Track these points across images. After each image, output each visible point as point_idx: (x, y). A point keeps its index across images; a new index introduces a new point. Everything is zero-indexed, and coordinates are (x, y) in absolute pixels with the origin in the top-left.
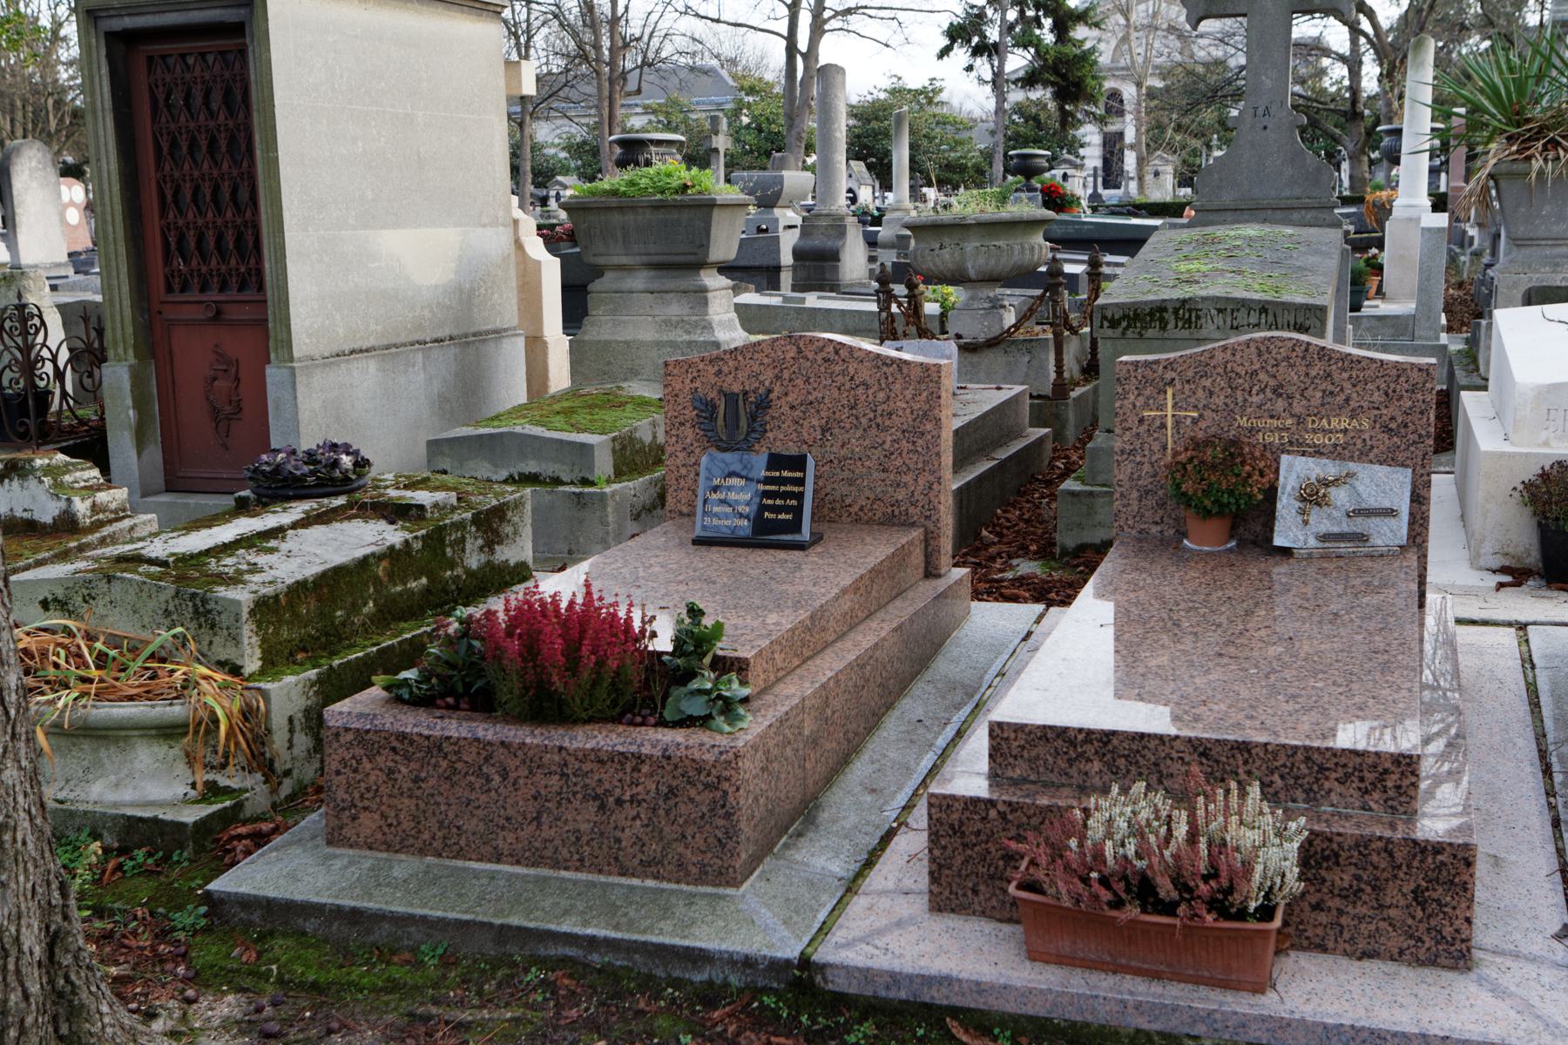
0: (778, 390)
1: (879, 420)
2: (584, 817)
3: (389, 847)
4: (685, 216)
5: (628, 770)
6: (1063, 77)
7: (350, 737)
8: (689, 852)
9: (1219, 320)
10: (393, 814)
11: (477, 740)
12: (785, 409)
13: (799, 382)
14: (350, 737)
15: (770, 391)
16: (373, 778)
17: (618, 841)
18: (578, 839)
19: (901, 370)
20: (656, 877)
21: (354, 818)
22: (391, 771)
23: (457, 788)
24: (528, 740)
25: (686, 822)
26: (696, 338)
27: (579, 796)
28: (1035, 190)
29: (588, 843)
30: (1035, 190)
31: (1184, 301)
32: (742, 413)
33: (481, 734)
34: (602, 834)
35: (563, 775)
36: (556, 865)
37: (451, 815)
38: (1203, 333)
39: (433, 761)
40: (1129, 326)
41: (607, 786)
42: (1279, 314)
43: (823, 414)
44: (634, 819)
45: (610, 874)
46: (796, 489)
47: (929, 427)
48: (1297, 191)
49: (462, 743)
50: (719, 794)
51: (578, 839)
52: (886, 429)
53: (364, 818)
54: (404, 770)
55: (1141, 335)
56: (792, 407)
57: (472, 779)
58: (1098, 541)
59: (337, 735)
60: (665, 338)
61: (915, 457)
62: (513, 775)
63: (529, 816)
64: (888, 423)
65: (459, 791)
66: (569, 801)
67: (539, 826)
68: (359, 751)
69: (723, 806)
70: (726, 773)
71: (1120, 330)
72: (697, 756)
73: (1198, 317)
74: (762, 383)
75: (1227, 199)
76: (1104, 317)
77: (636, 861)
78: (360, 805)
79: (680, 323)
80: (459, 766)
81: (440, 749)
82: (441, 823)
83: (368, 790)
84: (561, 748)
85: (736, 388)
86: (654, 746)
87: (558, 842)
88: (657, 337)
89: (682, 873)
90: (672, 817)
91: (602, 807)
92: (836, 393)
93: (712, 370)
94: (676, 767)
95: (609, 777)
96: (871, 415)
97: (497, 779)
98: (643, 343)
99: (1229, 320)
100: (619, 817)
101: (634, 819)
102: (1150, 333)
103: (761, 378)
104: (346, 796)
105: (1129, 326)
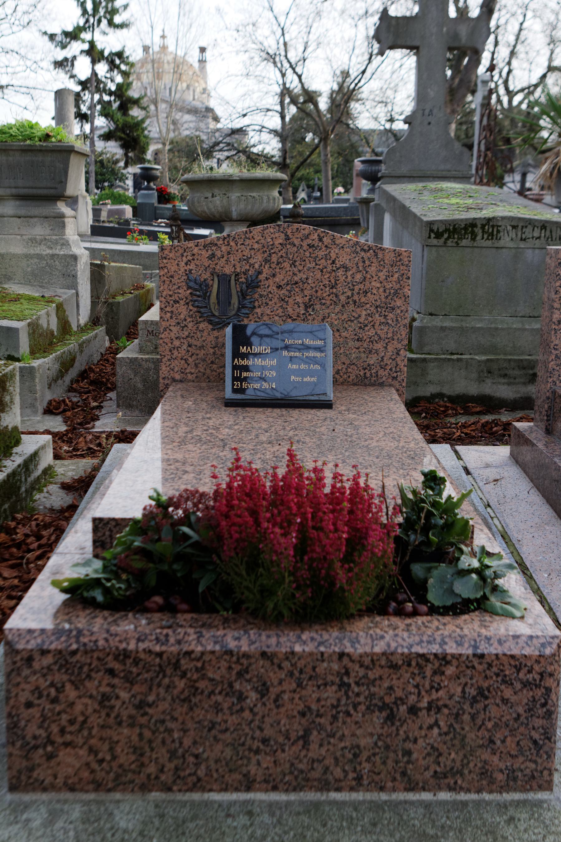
0: (266, 271)
1: (356, 298)
2: (367, 730)
3: (98, 786)
4: (48, 158)
5: (428, 673)
6: (128, 135)
7: (48, 660)
8: (495, 759)
9: (513, 234)
10: (106, 747)
11: (230, 653)
12: (273, 288)
13: (286, 265)
14: (48, 660)
16: (79, 708)
17: (408, 753)
18: (355, 756)
19: (376, 255)
20: (450, 789)
21: (50, 757)
22: (105, 697)
23: (197, 711)
24: (298, 648)
25: (496, 725)
26: (57, 252)
27: (362, 708)
28: (153, 189)
29: (368, 760)
30: (153, 189)
31: (489, 220)
32: (234, 292)
33: (232, 644)
34: (387, 747)
35: (342, 685)
36: (325, 786)
37: (187, 742)
38: (501, 243)
39: (166, 681)
40: (449, 237)
41: (399, 693)
42: (554, 229)
43: (306, 292)
44: (431, 727)
45: (394, 790)
47: (399, 303)
48: (448, 166)
49: (207, 658)
50: (539, 693)
51: (355, 756)
52: (361, 305)
53: (64, 755)
54: (124, 695)
55: (457, 243)
56: (279, 287)
57: (220, 698)
58: (428, 394)
59: (29, 660)
60: (32, 252)
61: (386, 329)
62: (274, 691)
63: (293, 736)
64: (363, 300)
65: (199, 713)
66: (348, 714)
67: (306, 745)
68: (59, 677)
69: (544, 705)
70: (550, 669)
71: (443, 240)
72: (515, 651)
73: (498, 232)
74: (252, 265)
75: (404, 170)
76: (431, 231)
77: (428, 774)
78: (59, 740)
79: (43, 241)
80: (201, 685)
81: (177, 666)
82: (173, 754)
83: (72, 722)
84: (342, 655)
85: (228, 270)
86: (459, 644)
87: (329, 761)
88: (25, 251)
89: (486, 780)
90: (479, 722)
91: (391, 718)
92: (319, 275)
93: (205, 254)
94: (490, 665)
95: (403, 684)
96: (349, 293)
97: (253, 695)
98: (14, 256)
99: (519, 234)
100: (412, 727)
101: (431, 727)
102: (464, 242)
103: (252, 261)
104: (42, 733)
105: (449, 237)
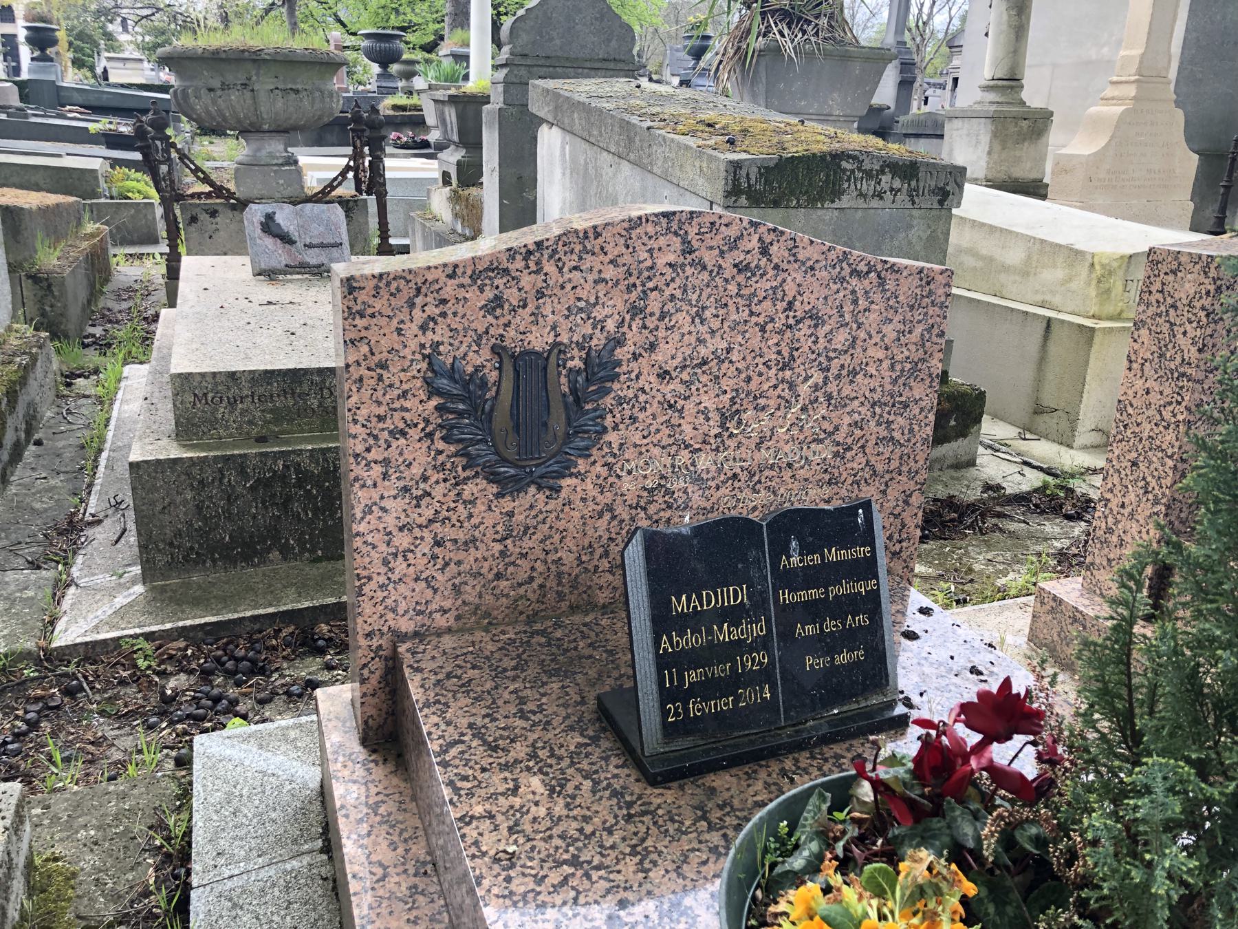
0: (634, 337)
1: (832, 387)
12: (649, 379)
13: (682, 319)
15: (619, 342)
43: (726, 384)
46: (861, 588)
56: (664, 375)
61: (886, 450)
74: (599, 324)
85: (539, 340)
92: (754, 336)
96: (817, 377)
103: (599, 313)
